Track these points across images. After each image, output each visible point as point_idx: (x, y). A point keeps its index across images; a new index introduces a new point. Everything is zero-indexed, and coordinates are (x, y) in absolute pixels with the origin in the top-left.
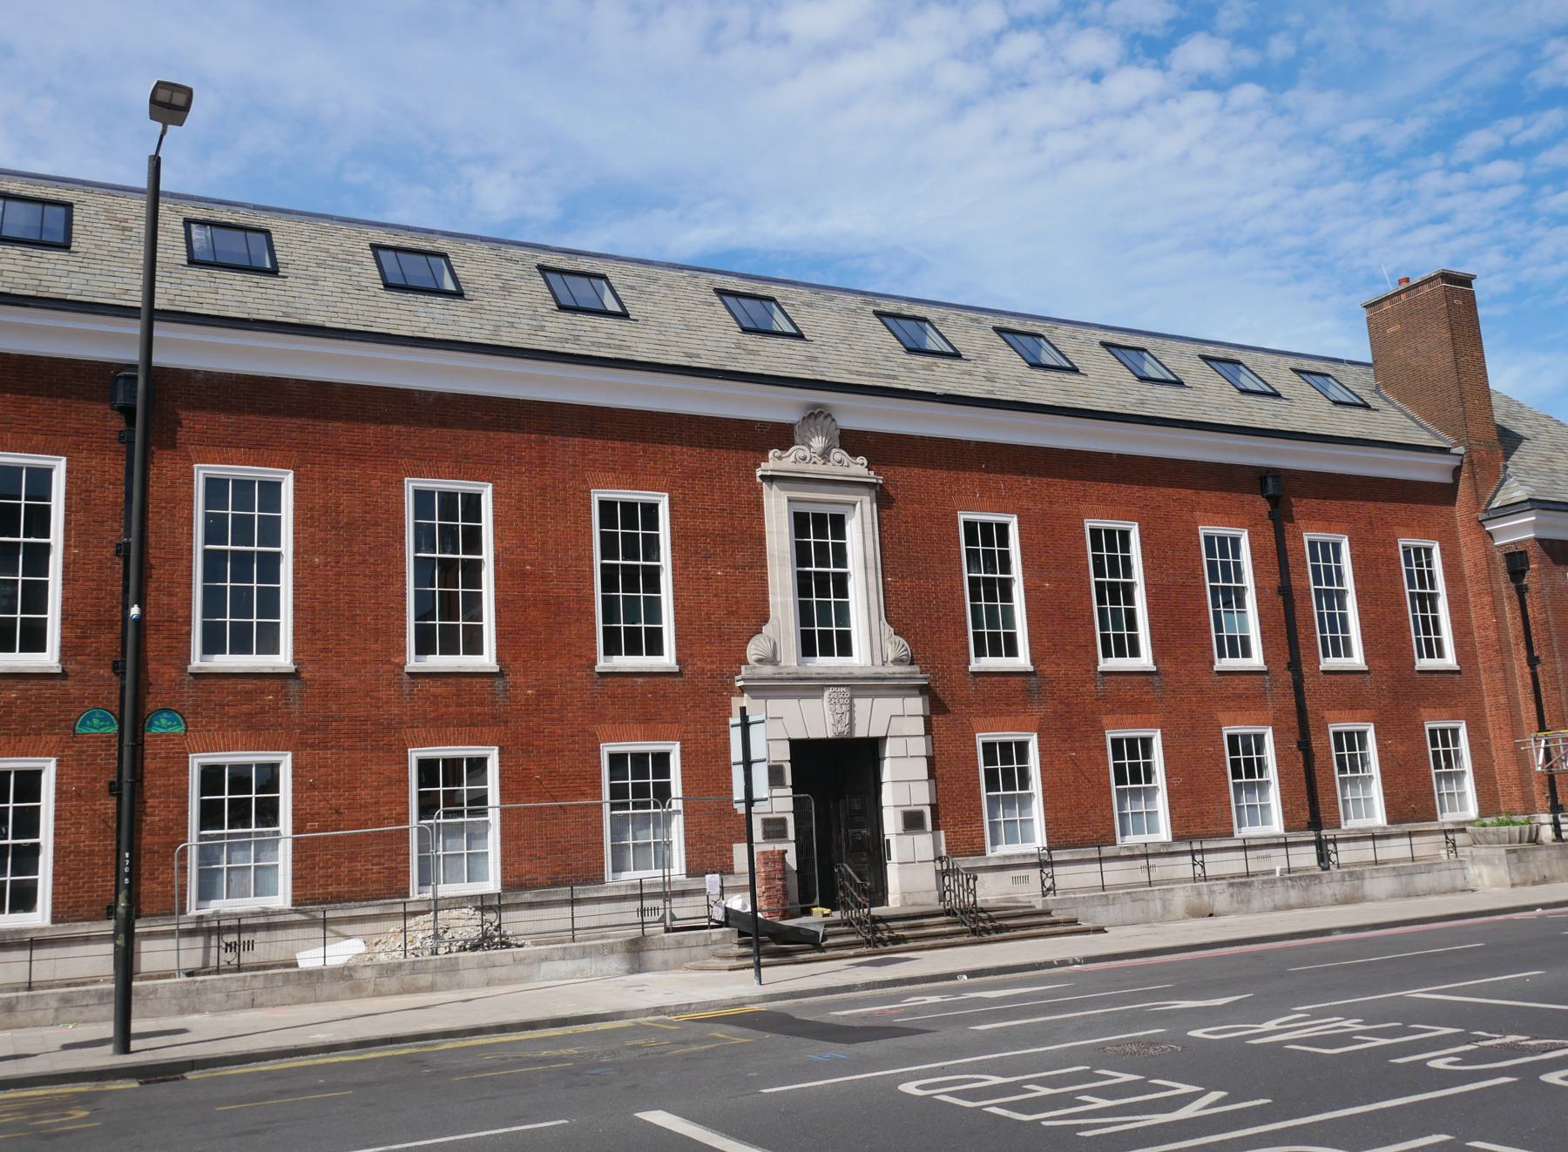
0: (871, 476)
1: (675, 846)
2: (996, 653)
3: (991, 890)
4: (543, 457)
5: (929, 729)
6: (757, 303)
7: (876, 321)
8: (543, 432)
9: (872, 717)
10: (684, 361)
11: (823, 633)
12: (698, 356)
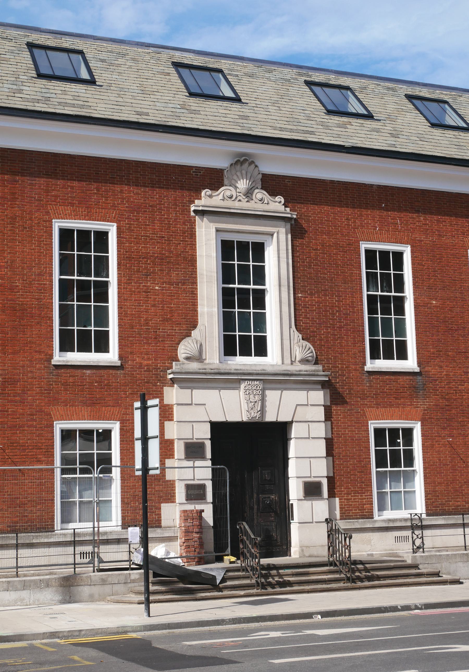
0: (287, 213)
1: (114, 504)
2: (388, 356)
3: (366, 546)
4: (14, 194)
5: (328, 416)
6: (337, 91)
7: (306, 89)
8: (14, 173)
9: (280, 406)
10: (133, 118)
11: (242, 337)
12: (147, 114)
